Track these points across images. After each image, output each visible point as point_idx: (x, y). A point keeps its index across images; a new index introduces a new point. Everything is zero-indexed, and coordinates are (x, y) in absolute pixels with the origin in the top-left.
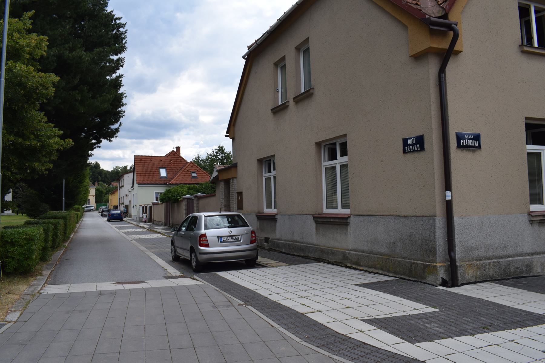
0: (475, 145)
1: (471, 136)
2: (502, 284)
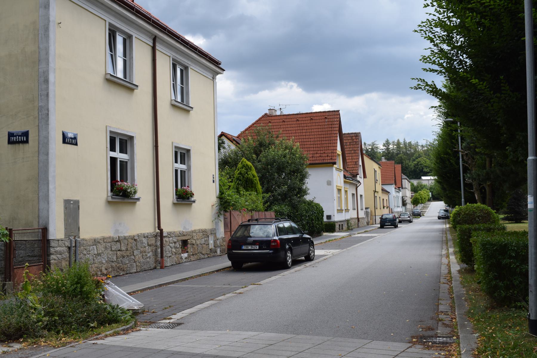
0: (22, 140)
1: (17, 140)
2: (122, 347)
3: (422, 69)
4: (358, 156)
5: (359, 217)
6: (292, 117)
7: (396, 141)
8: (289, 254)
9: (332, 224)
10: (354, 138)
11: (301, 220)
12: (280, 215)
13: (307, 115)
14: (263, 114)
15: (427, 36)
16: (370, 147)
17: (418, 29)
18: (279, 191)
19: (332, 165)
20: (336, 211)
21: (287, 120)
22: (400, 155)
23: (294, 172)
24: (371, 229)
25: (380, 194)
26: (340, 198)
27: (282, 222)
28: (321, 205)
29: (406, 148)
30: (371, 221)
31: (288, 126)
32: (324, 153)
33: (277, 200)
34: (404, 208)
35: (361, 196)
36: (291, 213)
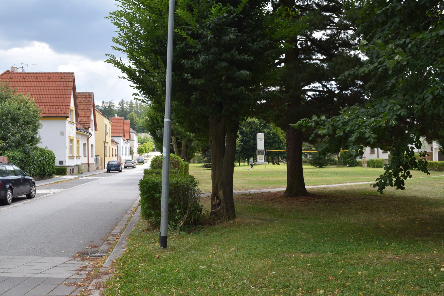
3: (112, 47)
4: (91, 112)
5: (89, 163)
6: (31, 75)
7: (129, 101)
8: (9, 193)
9: (64, 169)
10: (88, 96)
11: (32, 165)
12: (12, 159)
13: (45, 75)
14: (5, 70)
15: (116, 22)
16: (108, 105)
17: (108, 15)
18: (13, 139)
19: (65, 118)
20: (67, 158)
21: (27, 78)
22: (131, 113)
23: (28, 123)
24: (99, 173)
25: (109, 145)
26: (72, 147)
27: (5, 165)
28: (54, 152)
29: (137, 108)
30: (101, 166)
31: (28, 83)
32: (59, 108)
33: (11, 147)
34: (131, 156)
35: (92, 145)
36: (23, 158)
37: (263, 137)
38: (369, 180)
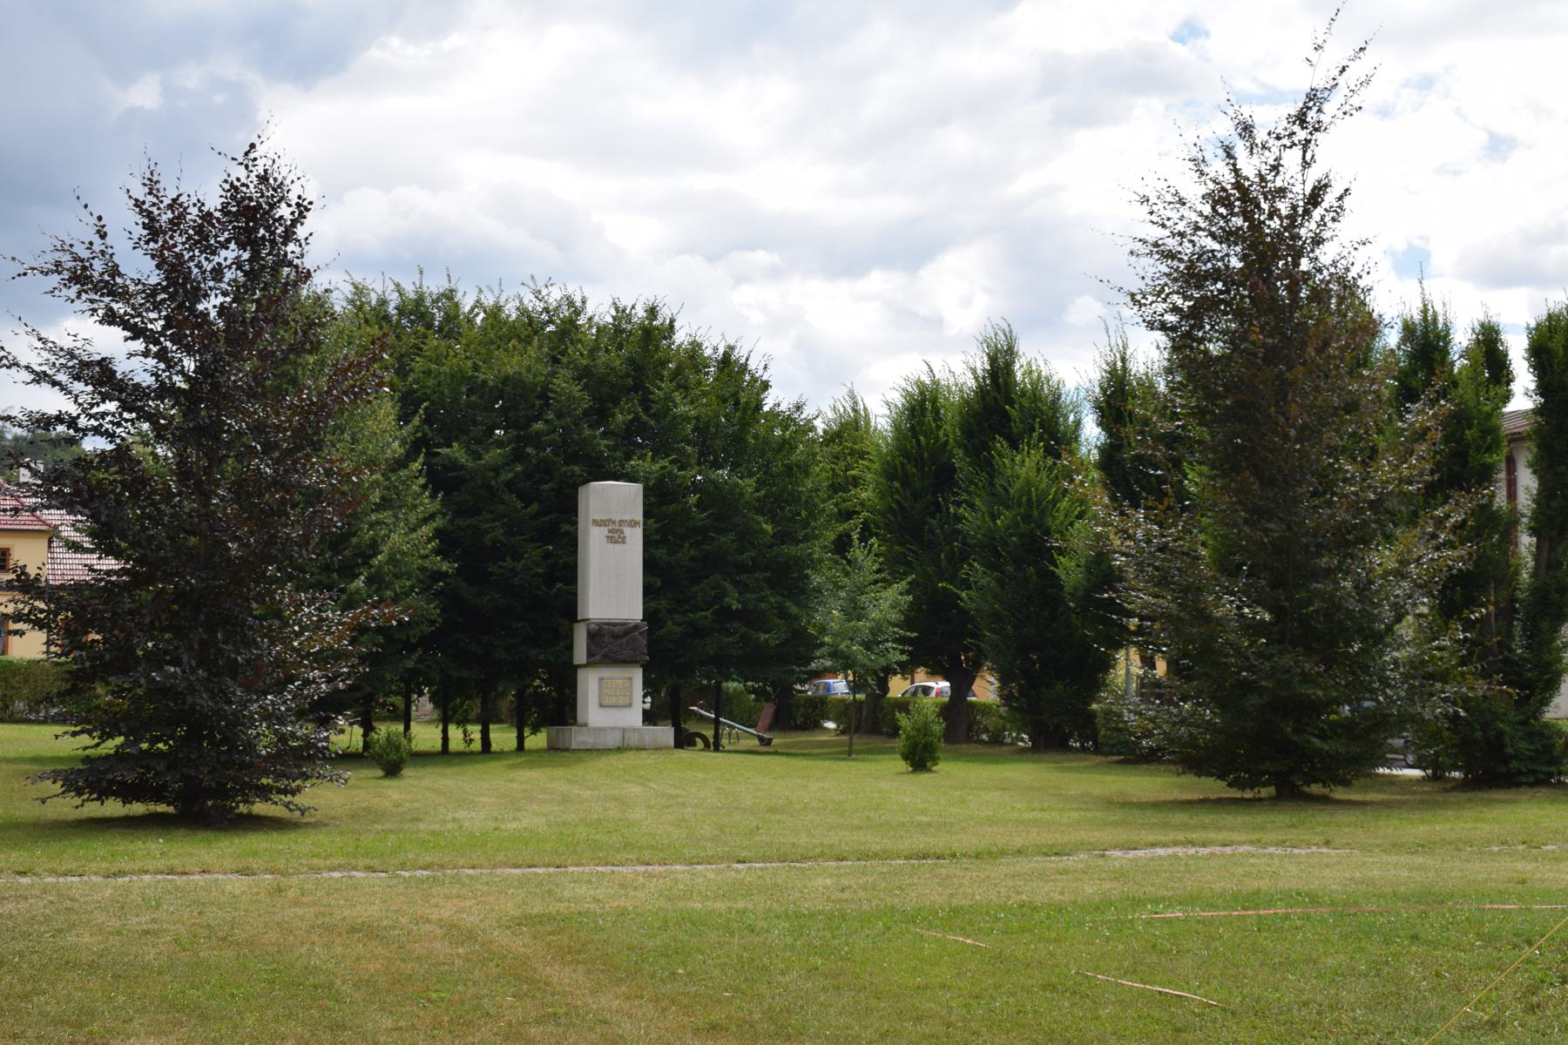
37: (640, 517)
38: (375, 863)
